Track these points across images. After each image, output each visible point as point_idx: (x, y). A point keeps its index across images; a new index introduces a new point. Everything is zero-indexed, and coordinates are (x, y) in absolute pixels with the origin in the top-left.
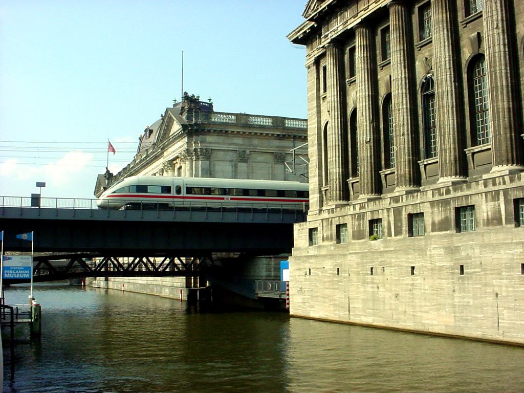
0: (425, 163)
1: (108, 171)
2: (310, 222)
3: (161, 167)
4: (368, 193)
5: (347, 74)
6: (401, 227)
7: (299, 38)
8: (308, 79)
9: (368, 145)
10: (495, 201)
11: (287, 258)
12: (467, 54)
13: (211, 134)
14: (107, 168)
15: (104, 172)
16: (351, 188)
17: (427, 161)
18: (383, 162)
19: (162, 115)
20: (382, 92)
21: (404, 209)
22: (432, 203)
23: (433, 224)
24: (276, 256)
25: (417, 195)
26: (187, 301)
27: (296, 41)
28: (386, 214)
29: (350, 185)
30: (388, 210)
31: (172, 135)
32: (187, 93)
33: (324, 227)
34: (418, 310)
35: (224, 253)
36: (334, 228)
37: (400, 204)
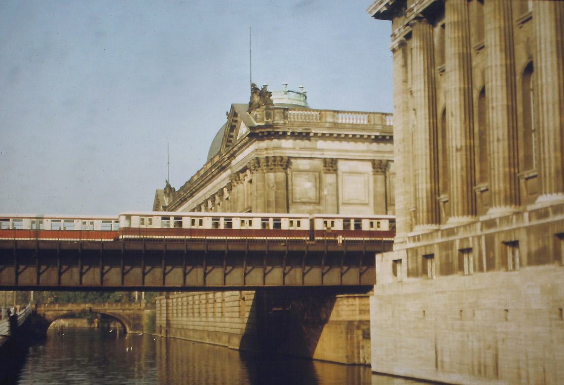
0: (526, 176)
1: (168, 186)
2: (398, 250)
3: (228, 181)
4: (458, 215)
5: (437, 60)
6: (494, 258)
7: (382, 12)
8: (393, 64)
9: (459, 154)
10: (449, 250)
11: (368, 297)
12: (521, 62)
13: (288, 137)
14: (167, 182)
15: (162, 186)
16: (442, 208)
17: (528, 174)
18: (478, 176)
19: (227, 113)
20: (478, 84)
21: (496, 236)
22: (529, 230)
23: (529, 255)
24: (362, 295)
25: (140, 297)
26: (239, 350)
27: (378, 16)
28: (476, 243)
29: (441, 204)
30: (479, 237)
31: (238, 140)
32: (255, 85)
33: (409, 259)
34: (163, 335)
35: (148, 310)
36: (420, 259)
37: (492, 231)
